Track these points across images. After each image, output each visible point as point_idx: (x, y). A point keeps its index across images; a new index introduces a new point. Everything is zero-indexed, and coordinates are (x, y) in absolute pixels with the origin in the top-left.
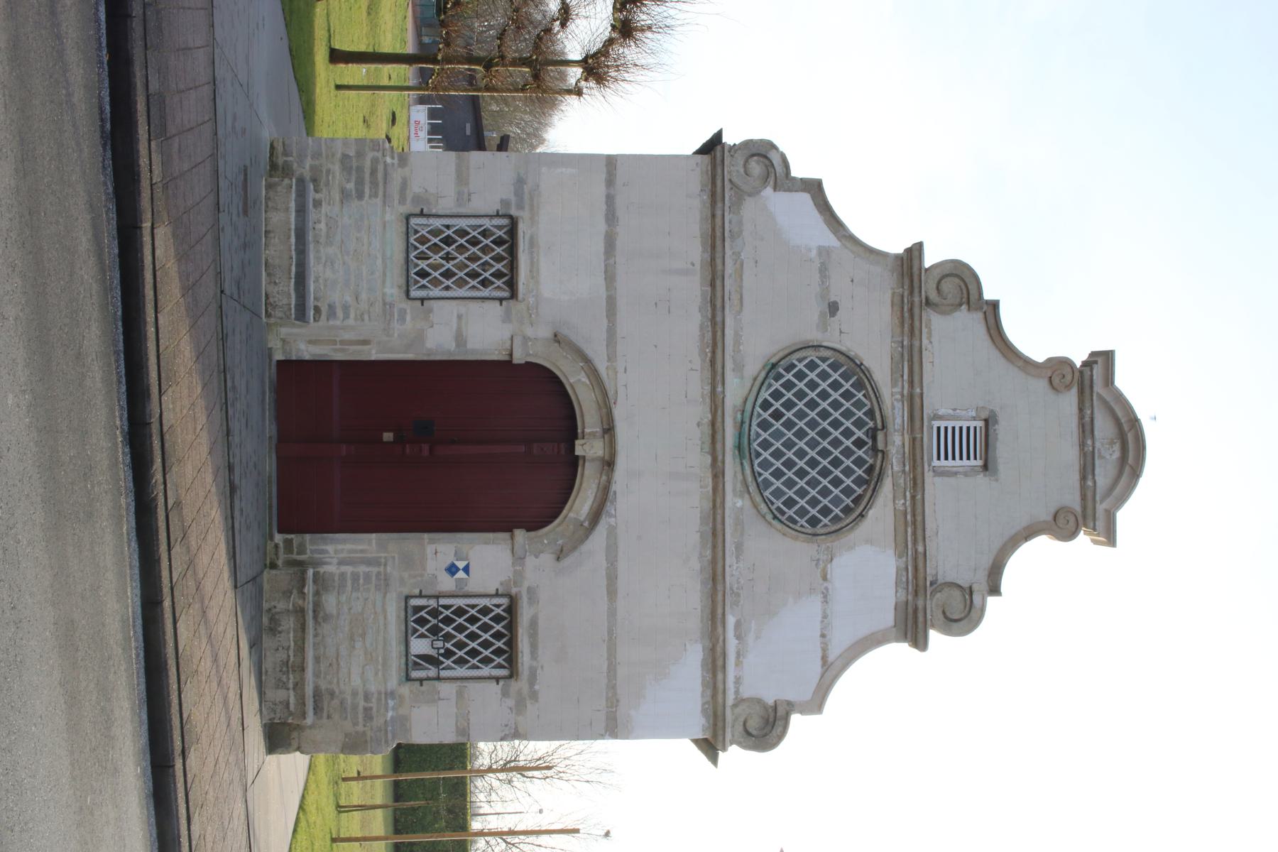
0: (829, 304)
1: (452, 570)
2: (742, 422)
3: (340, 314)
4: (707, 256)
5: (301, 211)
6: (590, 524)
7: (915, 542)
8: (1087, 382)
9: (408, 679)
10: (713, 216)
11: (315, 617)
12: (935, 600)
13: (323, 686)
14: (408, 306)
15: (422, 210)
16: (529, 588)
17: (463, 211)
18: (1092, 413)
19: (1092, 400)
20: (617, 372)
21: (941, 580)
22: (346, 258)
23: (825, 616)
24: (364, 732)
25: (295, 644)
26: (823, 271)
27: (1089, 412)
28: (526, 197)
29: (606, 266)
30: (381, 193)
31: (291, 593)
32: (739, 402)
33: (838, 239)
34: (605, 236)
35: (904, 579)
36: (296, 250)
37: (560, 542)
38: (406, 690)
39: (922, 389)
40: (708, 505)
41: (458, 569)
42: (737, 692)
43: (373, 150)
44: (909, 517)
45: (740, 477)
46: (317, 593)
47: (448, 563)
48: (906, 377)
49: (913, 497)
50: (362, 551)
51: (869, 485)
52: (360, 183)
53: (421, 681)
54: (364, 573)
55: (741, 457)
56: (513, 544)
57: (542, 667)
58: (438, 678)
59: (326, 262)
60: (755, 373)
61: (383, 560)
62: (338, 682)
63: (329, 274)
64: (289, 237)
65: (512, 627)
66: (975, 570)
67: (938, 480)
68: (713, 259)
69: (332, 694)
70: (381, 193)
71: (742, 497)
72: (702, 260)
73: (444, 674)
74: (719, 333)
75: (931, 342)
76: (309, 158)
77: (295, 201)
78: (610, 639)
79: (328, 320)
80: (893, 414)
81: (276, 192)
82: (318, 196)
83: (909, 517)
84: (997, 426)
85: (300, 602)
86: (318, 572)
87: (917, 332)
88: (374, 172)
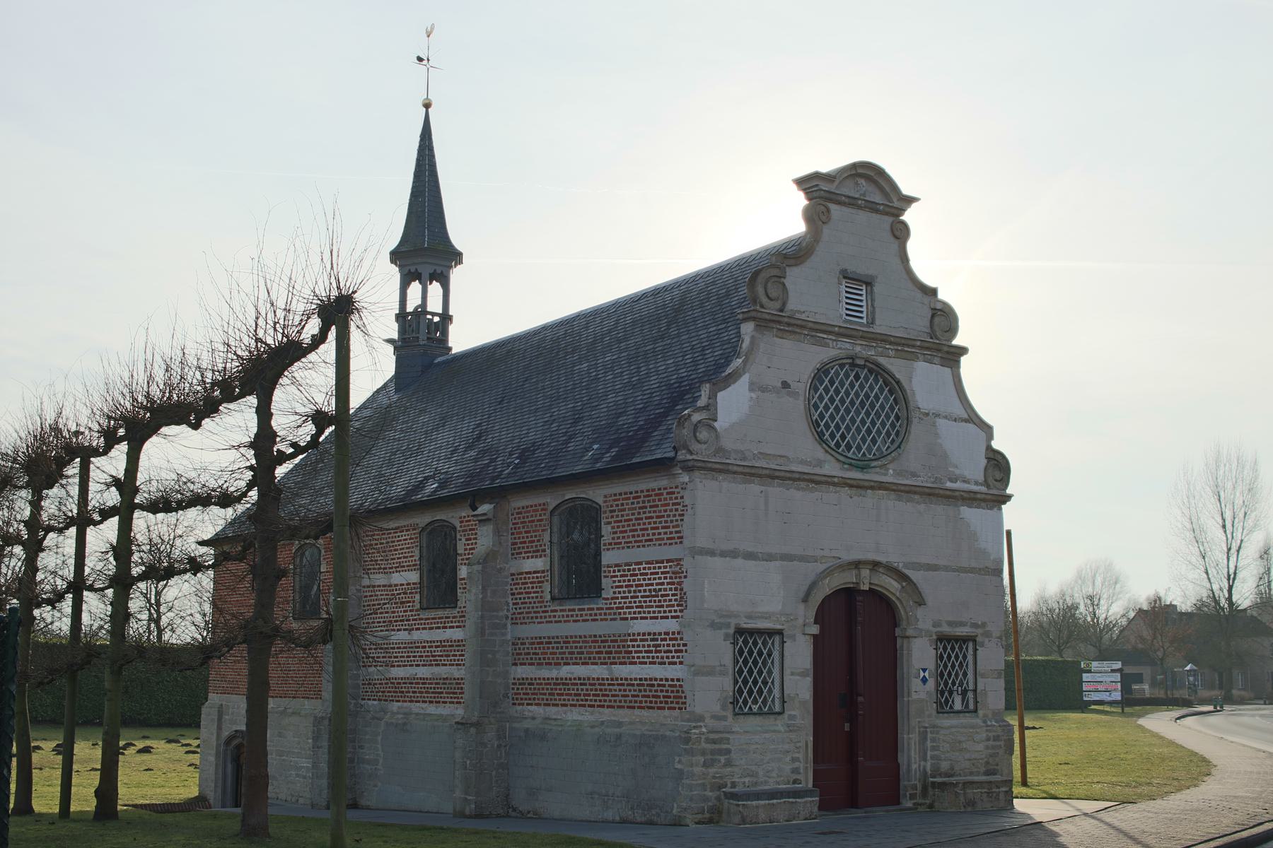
0: (783, 388)
1: (924, 680)
2: (850, 464)
3: (797, 764)
4: (757, 480)
5: (758, 796)
6: (906, 581)
7: (913, 346)
8: (827, 195)
9: (975, 711)
10: (735, 473)
11: (952, 776)
12: (941, 338)
13: (983, 769)
14: (787, 713)
15: (731, 703)
16: (934, 626)
17: (787, 672)
18: (845, 196)
19: (838, 194)
20: (823, 556)
21: (928, 330)
22: (765, 761)
23: (946, 417)
24: (1005, 740)
25: (978, 788)
26: (763, 389)
27: (843, 198)
28: (722, 620)
29: (763, 560)
30: (727, 736)
31: (956, 792)
32: (838, 465)
33: (744, 374)
34: (745, 559)
35: (929, 357)
36: (780, 799)
37: (911, 603)
38: (981, 712)
39: (837, 326)
40: (893, 495)
41: (924, 676)
42: (976, 483)
43: (700, 742)
44: (900, 348)
45: (878, 470)
46: (940, 775)
47: (920, 682)
48: (825, 336)
49: (891, 343)
50: (915, 744)
51: (880, 374)
52: (720, 752)
53: (976, 702)
54: (931, 742)
55: (868, 467)
56: (912, 637)
57: (971, 619)
58: (975, 691)
59: (768, 777)
60: (822, 451)
61: (922, 729)
62: (981, 759)
63: (774, 774)
64: (773, 804)
65: (752, 632)
66: (923, 304)
67: (877, 322)
68: (760, 476)
69: (987, 763)
70: (727, 736)
71: (888, 470)
72: (760, 485)
73: (971, 687)
74: (805, 477)
75: (804, 312)
76: (706, 793)
77: (752, 801)
78: (957, 571)
79: (800, 773)
80: (844, 349)
81: (747, 816)
82: (729, 785)
83: (900, 348)
84: (849, 271)
85: (960, 785)
86: (931, 774)
87: (804, 323)
88: (714, 742)
